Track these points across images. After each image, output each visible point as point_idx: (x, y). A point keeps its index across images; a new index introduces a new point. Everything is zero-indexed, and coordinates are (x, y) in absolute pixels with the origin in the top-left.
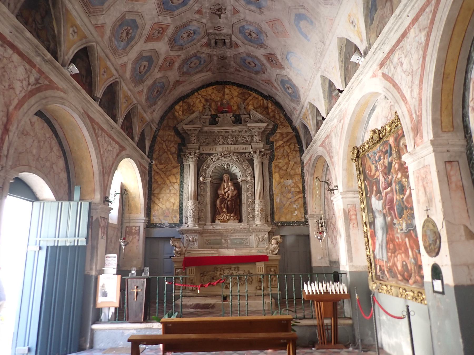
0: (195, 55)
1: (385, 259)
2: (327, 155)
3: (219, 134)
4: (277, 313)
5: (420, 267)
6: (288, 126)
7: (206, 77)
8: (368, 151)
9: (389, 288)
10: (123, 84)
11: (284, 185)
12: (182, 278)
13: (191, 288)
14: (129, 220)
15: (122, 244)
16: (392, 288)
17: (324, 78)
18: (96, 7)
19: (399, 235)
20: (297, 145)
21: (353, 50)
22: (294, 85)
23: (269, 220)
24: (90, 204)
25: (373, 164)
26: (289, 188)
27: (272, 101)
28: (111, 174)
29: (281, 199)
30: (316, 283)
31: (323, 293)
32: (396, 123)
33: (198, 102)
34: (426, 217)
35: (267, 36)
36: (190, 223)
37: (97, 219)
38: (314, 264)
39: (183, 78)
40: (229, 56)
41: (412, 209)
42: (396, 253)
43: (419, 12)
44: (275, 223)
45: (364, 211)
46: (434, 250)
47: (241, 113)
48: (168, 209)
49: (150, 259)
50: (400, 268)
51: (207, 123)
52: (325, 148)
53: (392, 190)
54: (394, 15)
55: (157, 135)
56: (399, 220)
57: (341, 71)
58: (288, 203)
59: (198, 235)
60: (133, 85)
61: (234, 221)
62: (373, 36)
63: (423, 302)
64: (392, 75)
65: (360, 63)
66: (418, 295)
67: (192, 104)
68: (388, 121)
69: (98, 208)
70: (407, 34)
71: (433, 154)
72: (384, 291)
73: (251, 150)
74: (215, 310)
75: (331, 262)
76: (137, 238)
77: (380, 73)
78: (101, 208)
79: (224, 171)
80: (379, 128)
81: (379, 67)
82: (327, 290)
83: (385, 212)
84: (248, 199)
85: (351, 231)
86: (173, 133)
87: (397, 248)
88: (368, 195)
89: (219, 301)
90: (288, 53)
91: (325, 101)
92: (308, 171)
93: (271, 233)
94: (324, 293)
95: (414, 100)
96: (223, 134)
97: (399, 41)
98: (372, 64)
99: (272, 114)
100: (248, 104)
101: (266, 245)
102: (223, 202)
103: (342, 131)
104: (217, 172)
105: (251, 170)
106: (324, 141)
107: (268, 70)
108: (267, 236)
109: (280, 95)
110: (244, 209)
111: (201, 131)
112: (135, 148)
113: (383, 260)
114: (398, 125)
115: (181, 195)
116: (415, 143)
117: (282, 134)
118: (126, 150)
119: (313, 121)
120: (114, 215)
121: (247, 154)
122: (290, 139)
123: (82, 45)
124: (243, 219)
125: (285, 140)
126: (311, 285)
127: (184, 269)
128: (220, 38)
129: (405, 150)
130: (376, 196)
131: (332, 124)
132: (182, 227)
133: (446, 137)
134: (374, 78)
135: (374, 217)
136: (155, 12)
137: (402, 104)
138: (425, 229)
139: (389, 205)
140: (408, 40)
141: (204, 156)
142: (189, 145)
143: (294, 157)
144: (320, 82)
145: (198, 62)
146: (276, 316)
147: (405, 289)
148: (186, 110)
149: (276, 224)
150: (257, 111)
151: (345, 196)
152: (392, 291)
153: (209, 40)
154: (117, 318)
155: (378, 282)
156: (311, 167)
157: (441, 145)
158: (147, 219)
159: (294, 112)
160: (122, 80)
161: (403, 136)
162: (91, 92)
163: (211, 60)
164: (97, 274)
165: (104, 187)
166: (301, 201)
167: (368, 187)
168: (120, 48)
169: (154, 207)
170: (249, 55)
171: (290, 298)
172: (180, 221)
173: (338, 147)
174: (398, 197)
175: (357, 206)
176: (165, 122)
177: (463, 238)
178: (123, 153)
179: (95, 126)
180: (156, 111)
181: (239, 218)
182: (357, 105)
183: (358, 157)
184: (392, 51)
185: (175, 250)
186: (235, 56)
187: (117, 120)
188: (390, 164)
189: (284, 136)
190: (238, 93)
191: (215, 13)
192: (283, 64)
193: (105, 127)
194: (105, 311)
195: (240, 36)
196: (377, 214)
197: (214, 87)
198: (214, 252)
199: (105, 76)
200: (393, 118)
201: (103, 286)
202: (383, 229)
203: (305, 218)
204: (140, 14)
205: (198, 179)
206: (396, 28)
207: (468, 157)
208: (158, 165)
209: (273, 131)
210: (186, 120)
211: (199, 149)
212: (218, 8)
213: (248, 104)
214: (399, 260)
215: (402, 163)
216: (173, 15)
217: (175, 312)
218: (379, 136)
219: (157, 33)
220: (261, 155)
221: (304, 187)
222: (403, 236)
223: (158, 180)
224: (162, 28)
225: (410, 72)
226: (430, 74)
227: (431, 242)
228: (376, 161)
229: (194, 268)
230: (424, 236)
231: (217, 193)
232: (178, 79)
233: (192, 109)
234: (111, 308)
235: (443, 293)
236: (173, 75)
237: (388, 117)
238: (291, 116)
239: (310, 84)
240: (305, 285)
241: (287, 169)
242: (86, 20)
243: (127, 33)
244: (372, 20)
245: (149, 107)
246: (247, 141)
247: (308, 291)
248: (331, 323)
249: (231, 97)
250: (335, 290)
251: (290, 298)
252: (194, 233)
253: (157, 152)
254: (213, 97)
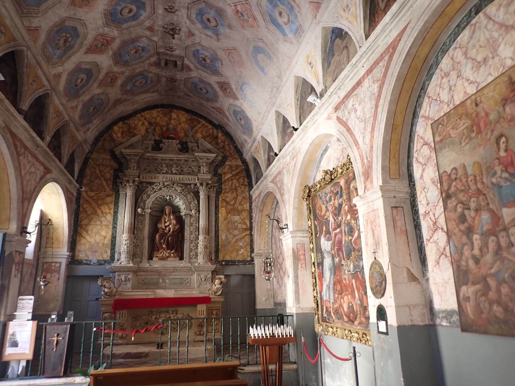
0: (141, 74)
1: (332, 301)
2: (278, 191)
3: (163, 162)
4: (220, 359)
5: (365, 308)
6: (238, 159)
7: (151, 98)
8: (319, 191)
9: (335, 330)
10: (55, 98)
11: (231, 220)
12: (114, 323)
13: (120, 334)
14: (52, 255)
15: (42, 283)
16: (338, 330)
17: (278, 114)
18: (31, 8)
19: (346, 276)
20: (246, 179)
21: (309, 90)
22: (247, 117)
23: (213, 258)
24: (5, 235)
25: (324, 204)
26: (236, 224)
27: (222, 130)
28: (32, 200)
29: (226, 236)
30: (262, 326)
31: (269, 337)
32: (348, 165)
33: (140, 125)
34: (374, 259)
35: (222, 64)
36: (123, 260)
37: (11, 254)
38: (259, 306)
39: (124, 97)
40: (179, 79)
41: (360, 250)
42: (343, 295)
43: (373, 65)
44: (219, 262)
45: (313, 252)
46: (380, 292)
47: (188, 141)
48: (98, 243)
49: (70, 300)
50: (346, 309)
51: (150, 149)
52: (277, 185)
53: (341, 232)
54: (350, 63)
55: (89, 158)
56: (347, 262)
57: (296, 109)
58: (234, 240)
59: (131, 274)
60: (66, 99)
61: (175, 259)
62: (330, 79)
63: (367, 343)
64: (347, 120)
65: (316, 104)
66: (363, 337)
67: (133, 126)
68: (340, 164)
69: (13, 240)
70: (361, 83)
71: (382, 199)
72: (330, 334)
73: (197, 181)
74: (148, 359)
75: (276, 304)
76: (57, 276)
77: (334, 116)
78: (18, 240)
79: (165, 203)
80: (331, 170)
81: (334, 110)
82: (273, 334)
83: (333, 253)
84: (191, 234)
85: (299, 271)
86: (109, 157)
87: (344, 289)
88: (318, 236)
89: (153, 349)
90: (244, 84)
91: (278, 136)
92: (257, 207)
93: (215, 273)
94: (270, 336)
95: (366, 146)
96: (166, 162)
97: (354, 89)
98: (328, 107)
99: (221, 145)
100: (196, 131)
101: (208, 286)
102: (162, 236)
103: (294, 169)
104: (159, 203)
105: (197, 203)
106: (275, 177)
107: (221, 99)
108: (210, 276)
109: (232, 126)
110: (186, 246)
111: (142, 157)
112: (62, 171)
113: (330, 302)
114: (349, 167)
115: (114, 228)
116: (365, 187)
117: (231, 167)
118: (52, 173)
119: (264, 156)
120: (30, 249)
121: (192, 186)
122: (240, 172)
123: (9, 48)
124: (185, 256)
125: (234, 173)
126: (257, 329)
127: (114, 313)
128: (171, 59)
129: (355, 193)
130: (325, 236)
131: (284, 161)
132: (113, 265)
133: (393, 183)
134: (329, 121)
135: (323, 258)
136: (100, 22)
137: (355, 148)
138: (372, 271)
139: (338, 245)
140: (362, 89)
141: (144, 184)
142: (127, 172)
143: (243, 192)
144: (274, 117)
145: (144, 81)
146: (219, 363)
147: (350, 331)
148: (126, 132)
149: (220, 263)
150: (205, 140)
151: (295, 235)
152: (338, 333)
153: (159, 59)
154: (29, 373)
155: (324, 324)
156: (260, 203)
157: (389, 191)
158: (71, 254)
159: (245, 145)
160: (54, 93)
161: (354, 178)
162: (15, 103)
163: (159, 81)
164: (6, 319)
165: (23, 215)
166: (247, 239)
167: (317, 227)
168: (55, 57)
169: (80, 241)
170: (202, 81)
171: (235, 344)
172: (111, 257)
173: (289, 185)
174: (346, 239)
175: (306, 246)
176: (100, 144)
177: (406, 280)
178: (48, 176)
179: (18, 143)
180: (90, 130)
181: (180, 255)
182: (311, 144)
183: (309, 196)
184: (347, 97)
185: (104, 291)
186: (186, 80)
187: (44, 138)
188: (340, 205)
189: (233, 169)
190: (186, 119)
191: (168, 33)
192: (237, 94)
193: (29, 144)
194: (13, 364)
195: (193, 60)
196: (326, 255)
197: (159, 110)
198: (149, 293)
199: (34, 87)
200: (345, 160)
201: (13, 335)
202: (331, 269)
203: (251, 257)
204: (82, 22)
205: (136, 210)
206: (351, 76)
207: (411, 204)
208: (89, 192)
209: (222, 163)
210: (126, 143)
211: (139, 177)
212: (171, 27)
213: (196, 131)
214: (345, 302)
215: (352, 205)
216: (121, 28)
217: (103, 363)
218: (331, 177)
219: (100, 45)
220: (208, 187)
221: (251, 223)
222: (350, 277)
223: (87, 209)
224: (107, 41)
225: (363, 119)
226: (381, 124)
227: (377, 284)
228: (327, 202)
229: (125, 312)
230: (371, 277)
231: (156, 226)
232: (119, 97)
233: (133, 131)
234: (21, 361)
235: (387, 334)
236: (114, 92)
237: (339, 159)
238: (242, 148)
239: (264, 118)
240: (251, 328)
241: (235, 204)
242: (17, 21)
243: (66, 41)
244: (329, 64)
245: (83, 125)
246: (193, 171)
247: (254, 335)
248: (276, 369)
249: (178, 122)
250: (282, 334)
251: (235, 344)
252: (128, 271)
253: (88, 177)
254: (158, 121)
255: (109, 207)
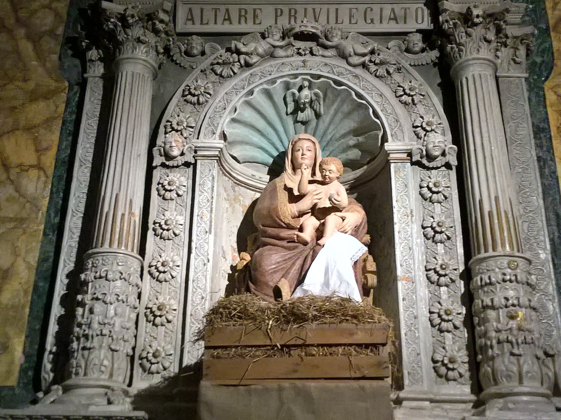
255: (36, 141)
